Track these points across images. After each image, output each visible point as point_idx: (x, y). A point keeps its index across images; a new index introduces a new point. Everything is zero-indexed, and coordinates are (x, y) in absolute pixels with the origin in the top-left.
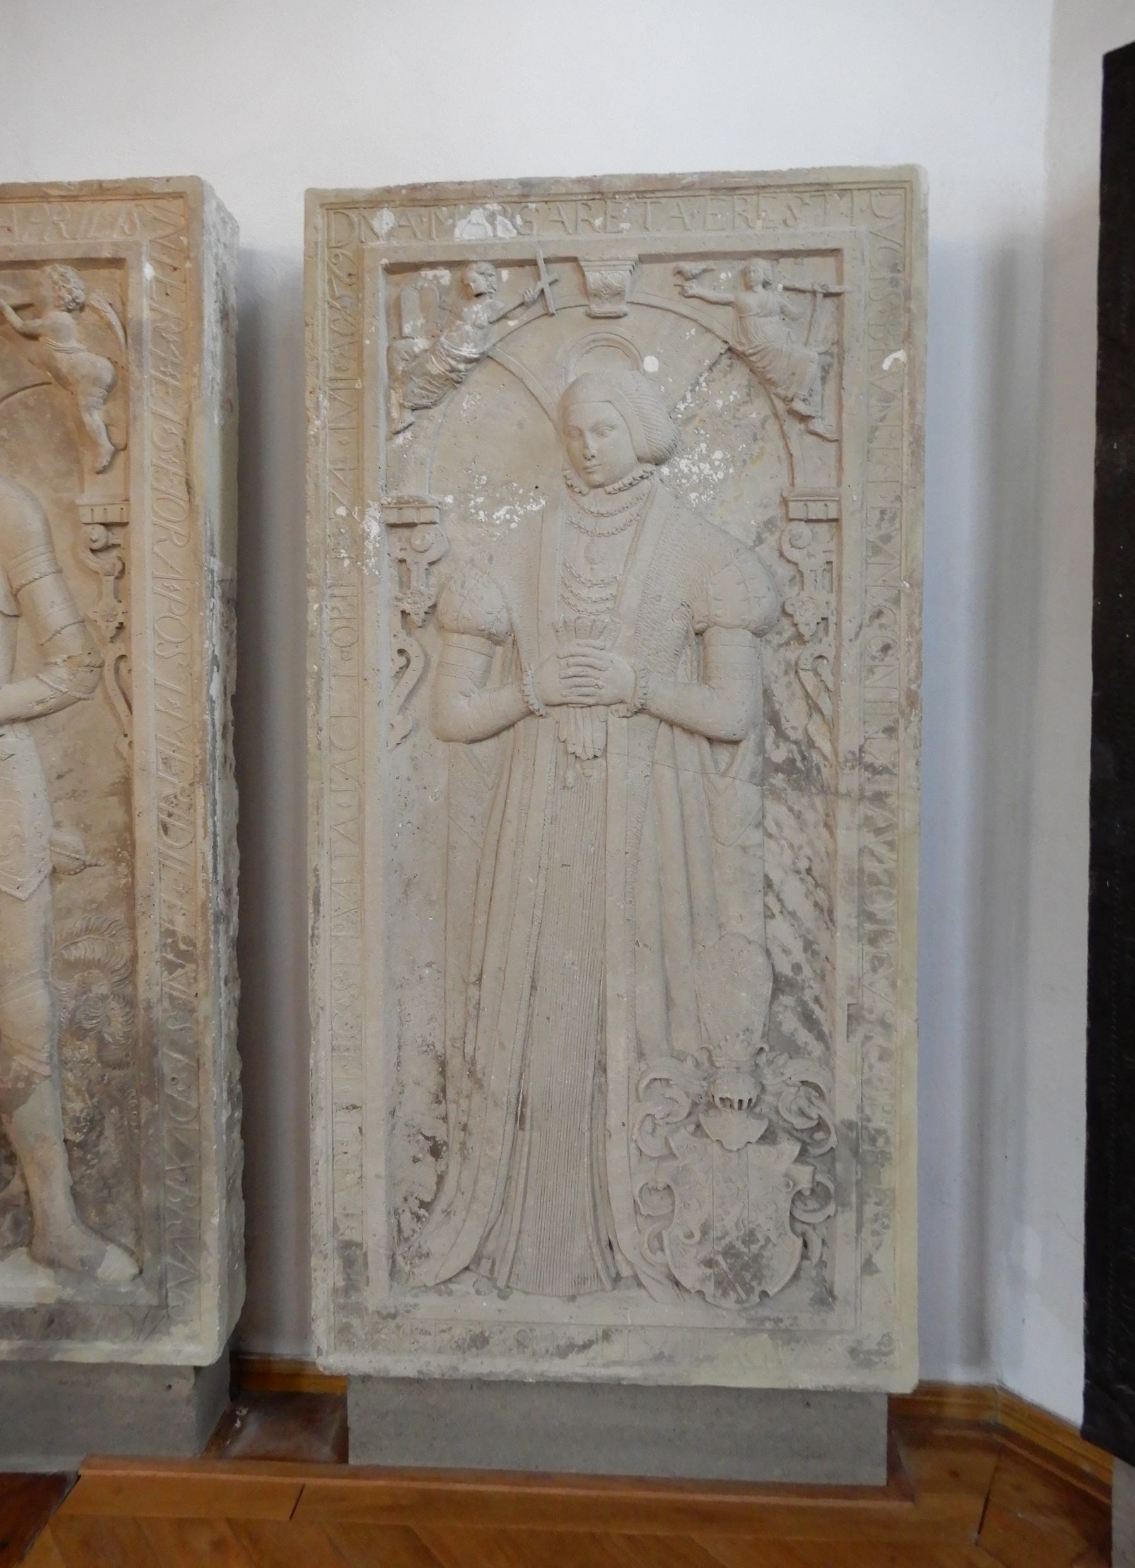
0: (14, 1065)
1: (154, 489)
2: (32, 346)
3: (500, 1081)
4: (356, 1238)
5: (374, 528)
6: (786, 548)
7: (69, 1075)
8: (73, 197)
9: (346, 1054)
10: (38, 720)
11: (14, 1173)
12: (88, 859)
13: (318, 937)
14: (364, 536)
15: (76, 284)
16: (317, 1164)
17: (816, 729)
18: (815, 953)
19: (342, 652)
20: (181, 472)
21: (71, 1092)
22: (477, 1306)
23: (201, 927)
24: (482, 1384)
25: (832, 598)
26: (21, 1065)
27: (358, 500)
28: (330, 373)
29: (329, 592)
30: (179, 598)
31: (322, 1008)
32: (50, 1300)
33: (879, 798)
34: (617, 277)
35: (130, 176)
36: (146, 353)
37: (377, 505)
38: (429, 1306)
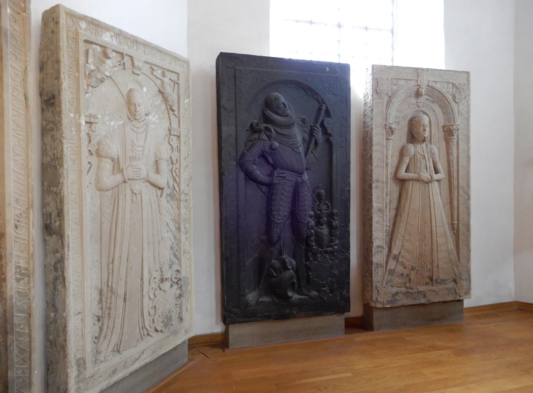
1: (12, 95)
3: (121, 291)
6: (170, 141)
18: (176, 239)
20: (22, 91)
22: (117, 359)
25: (178, 154)
27: (78, 111)
34: (141, 65)
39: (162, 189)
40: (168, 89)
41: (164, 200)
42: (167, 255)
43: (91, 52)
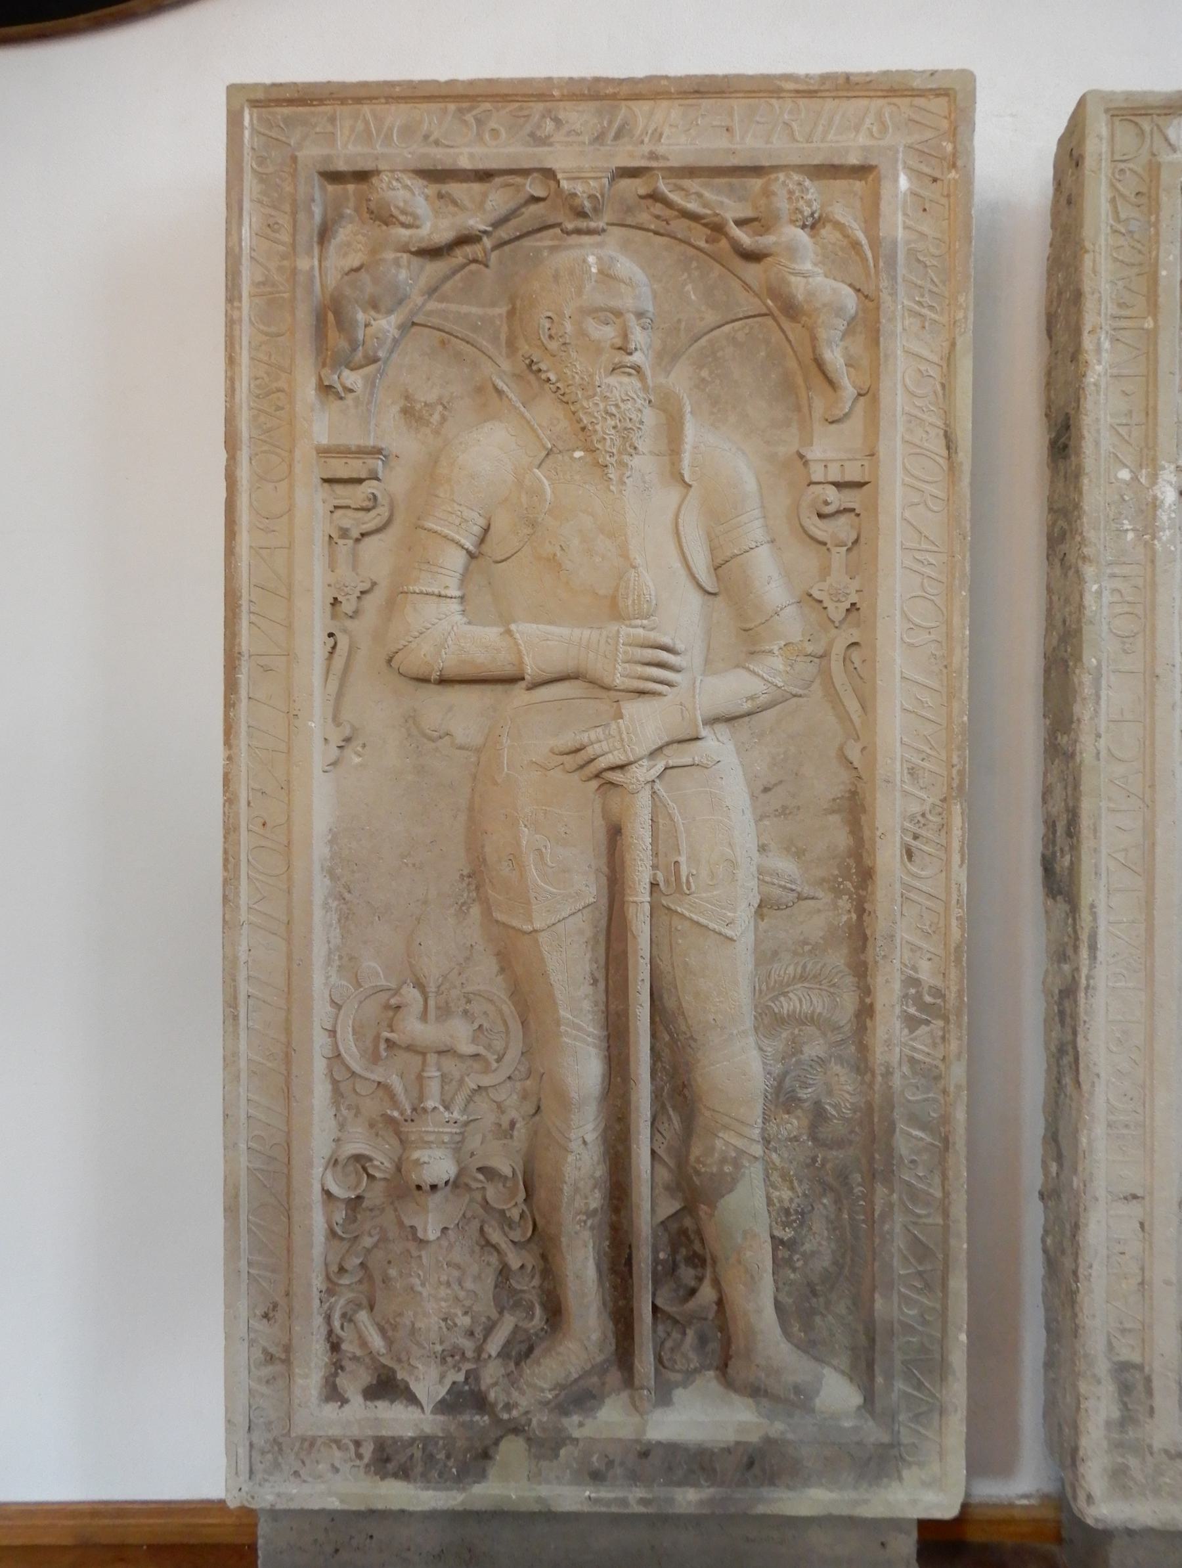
0: (719, 1144)
2: (752, 272)
4: (1136, 1358)
7: (774, 1156)
8: (810, 92)
9: (1125, 1131)
10: (741, 720)
11: (700, 1279)
12: (807, 890)
13: (1094, 988)
14: (1155, 504)
15: (814, 194)
16: (1091, 1267)
19: (1124, 643)
20: (940, 423)
21: (775, 1177)
23: (953, 973)
26: (727, 1143)
27: (1148, 459)
28: (1112, 309)
29: (1109, 571)
30: (933, 575)
31: (1098, 1075)
32: (754, 1438)
35: (884, 68)
36: (900, 280)
37: (1173, 467)
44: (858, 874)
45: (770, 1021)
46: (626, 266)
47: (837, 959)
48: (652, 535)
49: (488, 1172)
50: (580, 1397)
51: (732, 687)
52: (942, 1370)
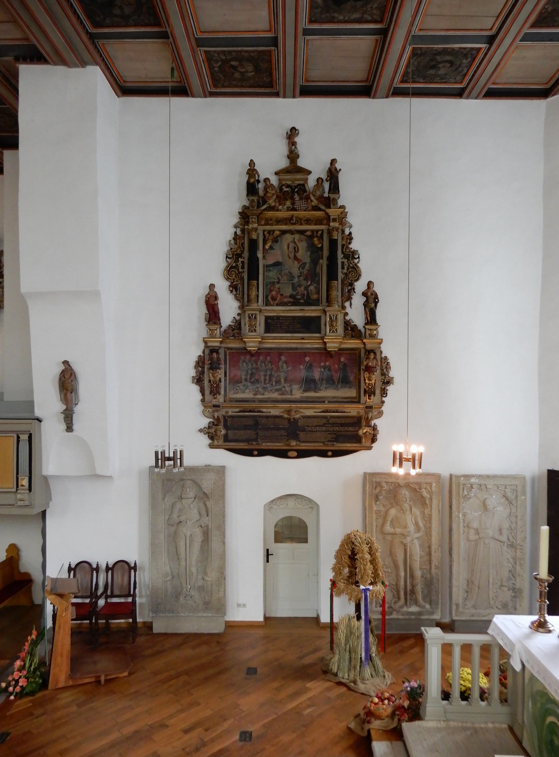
3: (476, 583)
5: (461, 516)
17: (514, 541)
22: (473, 611)
24: (473, 621)
27: (459, 512)
33: (522, 549)
34: (490, 487)
38: (467, 611)
39: (504, 542)
40: (509, 494)
41: (505, 548)
42: (506, 574)
43: (465, 488)
44: (430, 554)
45: (421, 569)
46: (407, 493)
47: (428, 562)
48: (409, 520)
49: (392, 584)
50: (401, 607)
51: (417, 535)
52: (438, 604)
